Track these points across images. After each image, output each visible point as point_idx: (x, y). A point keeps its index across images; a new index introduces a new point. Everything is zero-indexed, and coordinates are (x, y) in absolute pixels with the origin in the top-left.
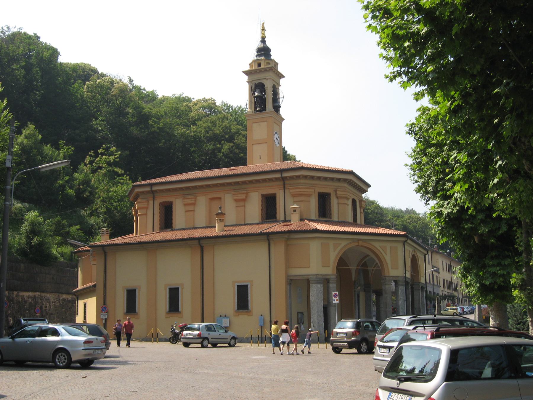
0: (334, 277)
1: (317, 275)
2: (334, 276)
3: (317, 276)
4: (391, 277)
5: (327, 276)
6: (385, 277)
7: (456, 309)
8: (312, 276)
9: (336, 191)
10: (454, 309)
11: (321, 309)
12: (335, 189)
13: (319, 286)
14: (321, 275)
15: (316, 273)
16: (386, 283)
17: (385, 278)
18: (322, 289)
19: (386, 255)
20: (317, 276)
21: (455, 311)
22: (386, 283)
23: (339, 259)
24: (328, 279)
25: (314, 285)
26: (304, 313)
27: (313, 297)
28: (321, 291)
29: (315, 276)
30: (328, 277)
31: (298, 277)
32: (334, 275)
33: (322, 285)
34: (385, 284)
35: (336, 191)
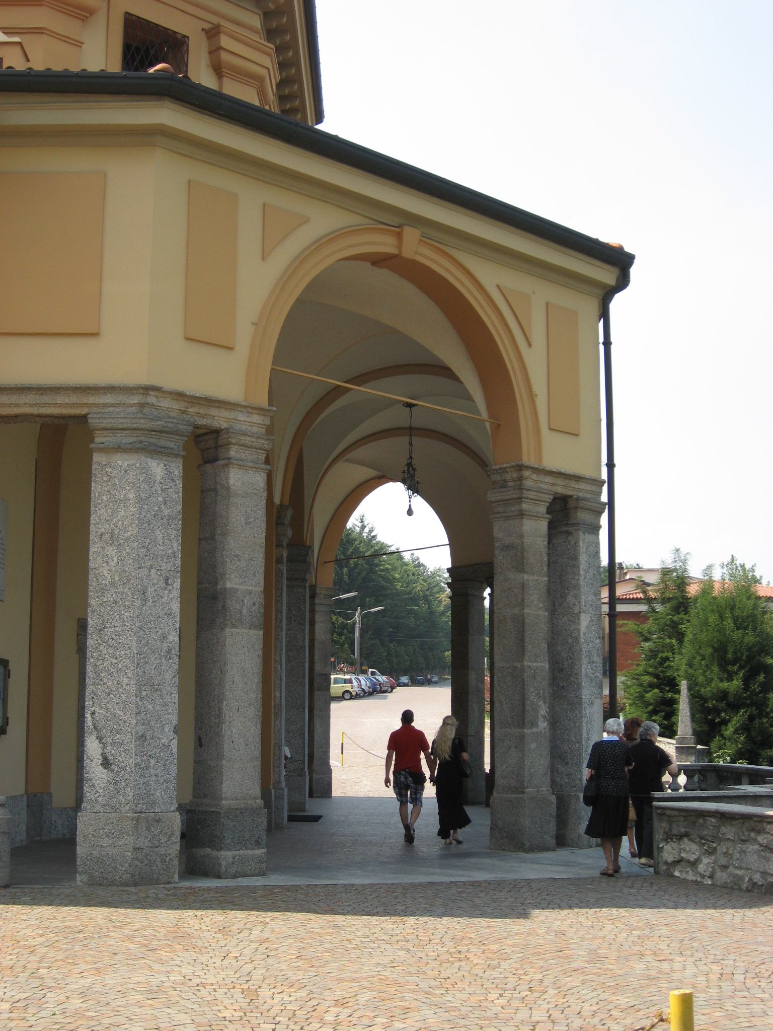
0: (252, 423)
1: (147, 389)
2: (256, 418)
3: (151, 399)
4: (551, 473)
5: (214, 412)
6: (520, 467)
7: (350, 681)
8: (108, 399)
9: (213, 33)
10: (346, 681)
11: (164, 637)
12: (207, 26)
13: (157, 468)
14: (179, 395)
15: (145, 381)
16: (524, 506)
17: (520, 479)
18: (176, 492)
19: (530, 345)
20: (151, 399)
21: (347, 687)
22: (524, 506)
23: (288, 317)
24: (217, 432)
25: (122, 461)
26: (11, 667)
27: (111, 551)
28: (166, 512)
29: (136, 399)
30: (220, 419)
31: (30, 398)
32: (261, 410)
33: (177, 468)
34: (521, 515)
35: (213, 33)
